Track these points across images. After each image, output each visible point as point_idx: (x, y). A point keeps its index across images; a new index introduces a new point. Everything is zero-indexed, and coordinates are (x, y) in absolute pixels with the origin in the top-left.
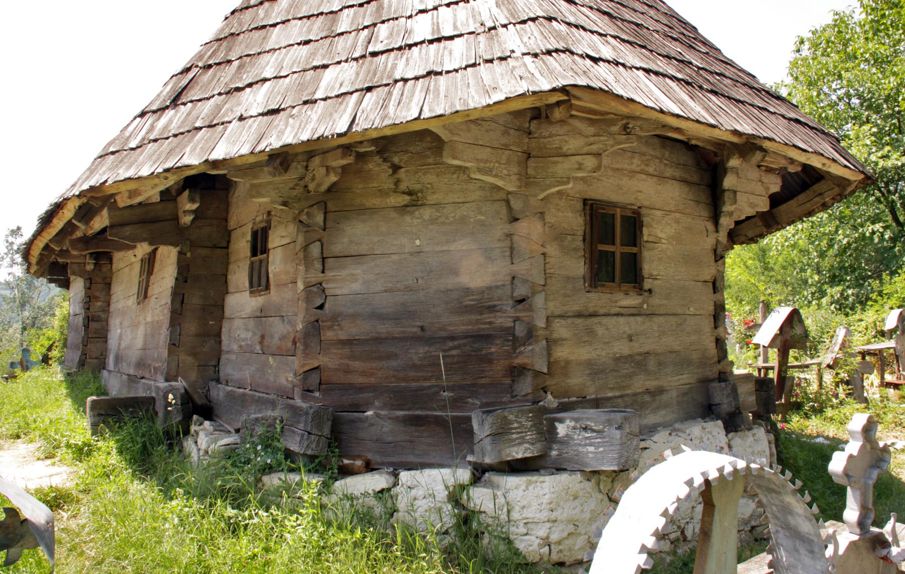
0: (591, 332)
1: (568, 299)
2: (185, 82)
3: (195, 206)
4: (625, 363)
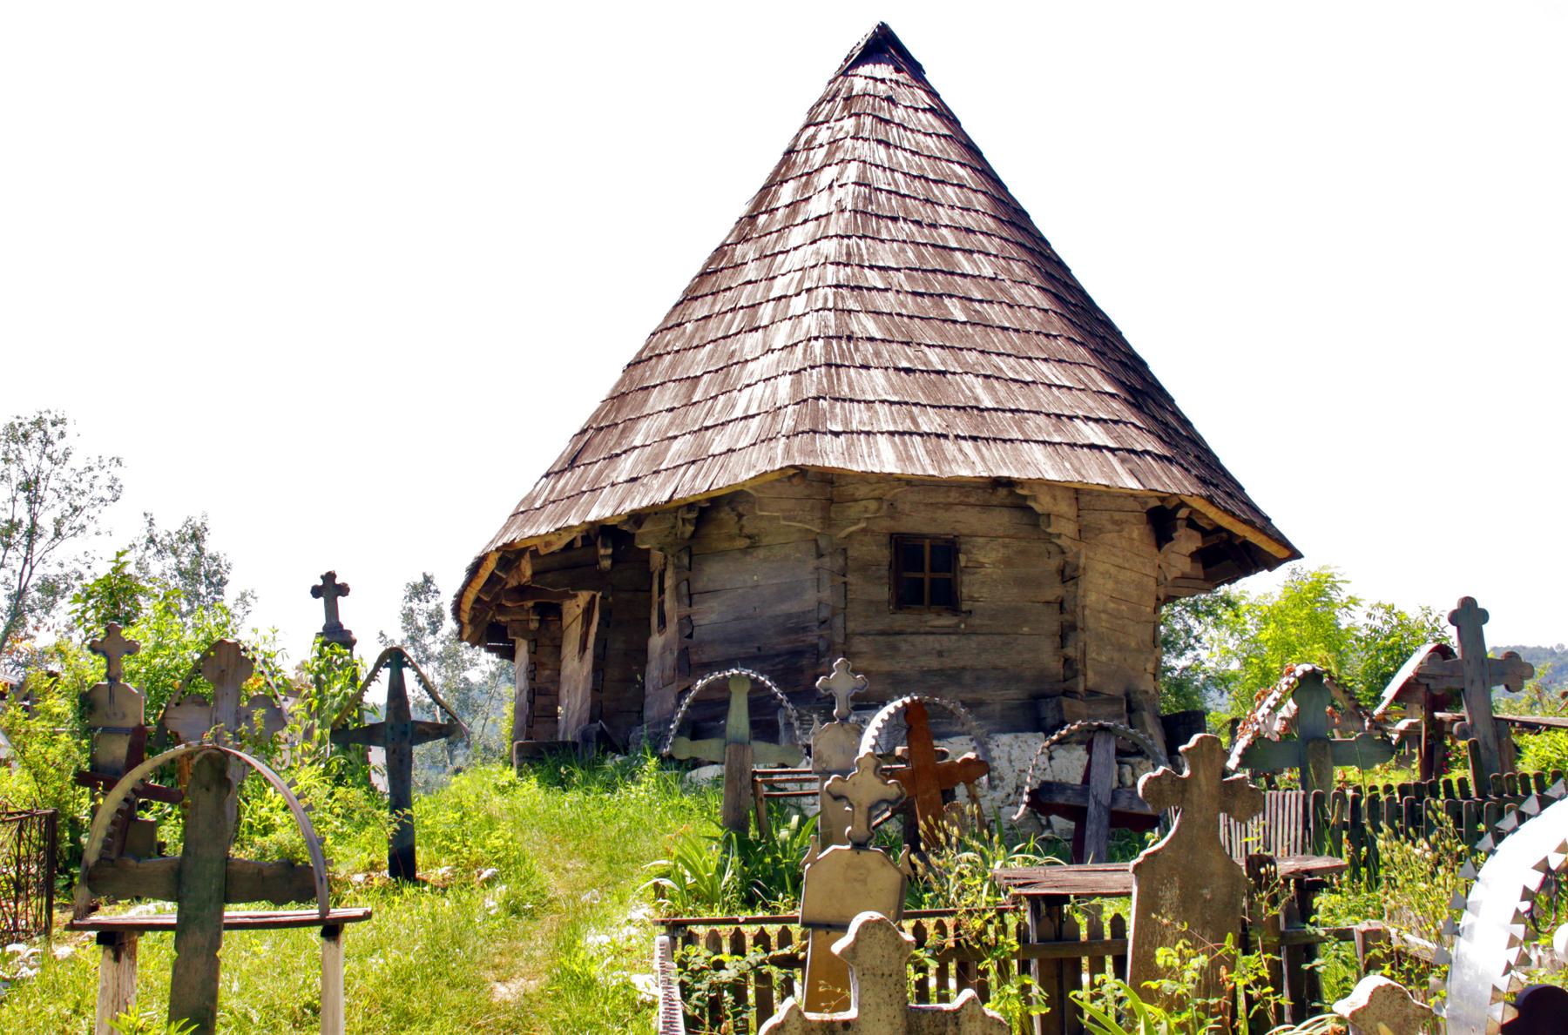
0: (894, 649)
2: (581, 444)
3: (609, 551)
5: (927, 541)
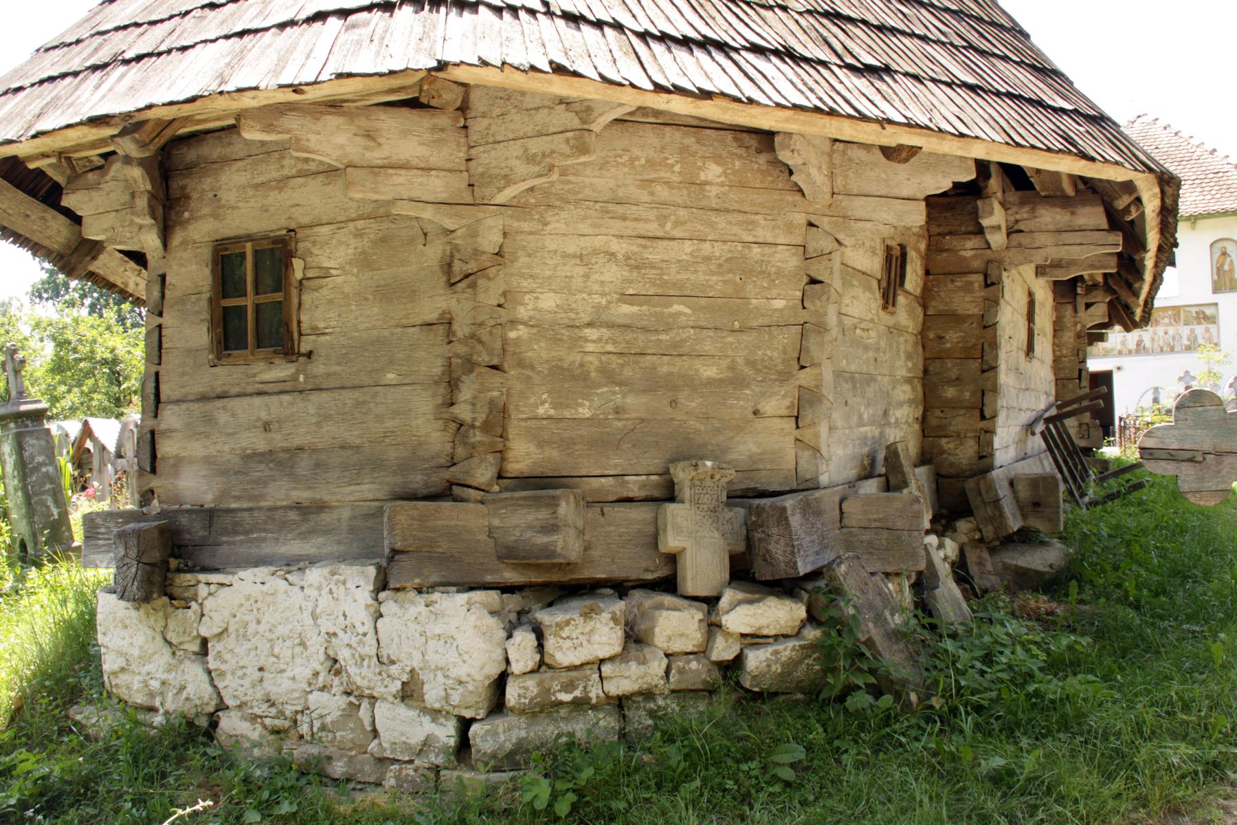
0: (209, 420)
1: (186, 378)
4: (261, 462)
5: (249, 245)
